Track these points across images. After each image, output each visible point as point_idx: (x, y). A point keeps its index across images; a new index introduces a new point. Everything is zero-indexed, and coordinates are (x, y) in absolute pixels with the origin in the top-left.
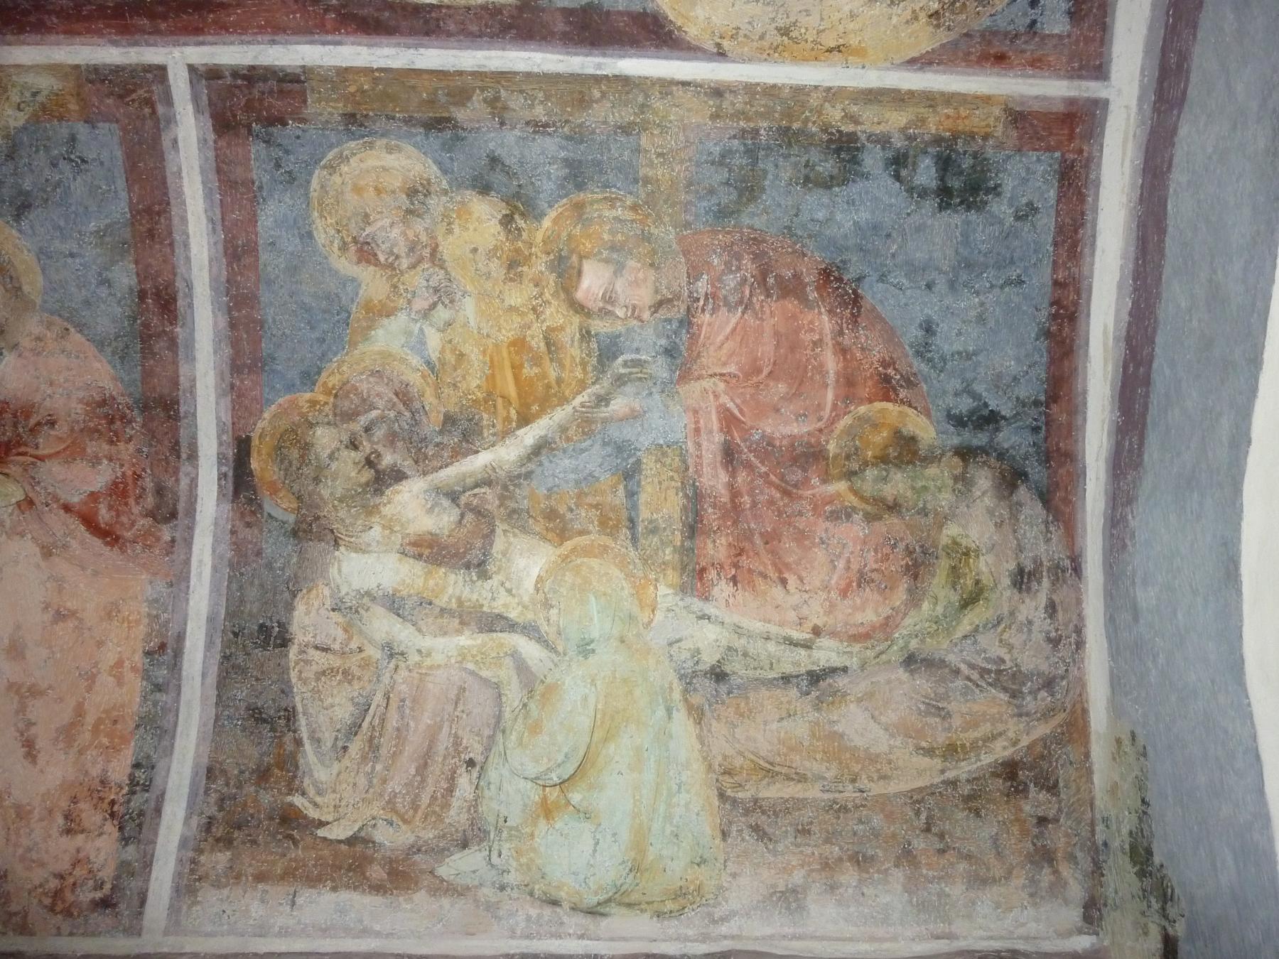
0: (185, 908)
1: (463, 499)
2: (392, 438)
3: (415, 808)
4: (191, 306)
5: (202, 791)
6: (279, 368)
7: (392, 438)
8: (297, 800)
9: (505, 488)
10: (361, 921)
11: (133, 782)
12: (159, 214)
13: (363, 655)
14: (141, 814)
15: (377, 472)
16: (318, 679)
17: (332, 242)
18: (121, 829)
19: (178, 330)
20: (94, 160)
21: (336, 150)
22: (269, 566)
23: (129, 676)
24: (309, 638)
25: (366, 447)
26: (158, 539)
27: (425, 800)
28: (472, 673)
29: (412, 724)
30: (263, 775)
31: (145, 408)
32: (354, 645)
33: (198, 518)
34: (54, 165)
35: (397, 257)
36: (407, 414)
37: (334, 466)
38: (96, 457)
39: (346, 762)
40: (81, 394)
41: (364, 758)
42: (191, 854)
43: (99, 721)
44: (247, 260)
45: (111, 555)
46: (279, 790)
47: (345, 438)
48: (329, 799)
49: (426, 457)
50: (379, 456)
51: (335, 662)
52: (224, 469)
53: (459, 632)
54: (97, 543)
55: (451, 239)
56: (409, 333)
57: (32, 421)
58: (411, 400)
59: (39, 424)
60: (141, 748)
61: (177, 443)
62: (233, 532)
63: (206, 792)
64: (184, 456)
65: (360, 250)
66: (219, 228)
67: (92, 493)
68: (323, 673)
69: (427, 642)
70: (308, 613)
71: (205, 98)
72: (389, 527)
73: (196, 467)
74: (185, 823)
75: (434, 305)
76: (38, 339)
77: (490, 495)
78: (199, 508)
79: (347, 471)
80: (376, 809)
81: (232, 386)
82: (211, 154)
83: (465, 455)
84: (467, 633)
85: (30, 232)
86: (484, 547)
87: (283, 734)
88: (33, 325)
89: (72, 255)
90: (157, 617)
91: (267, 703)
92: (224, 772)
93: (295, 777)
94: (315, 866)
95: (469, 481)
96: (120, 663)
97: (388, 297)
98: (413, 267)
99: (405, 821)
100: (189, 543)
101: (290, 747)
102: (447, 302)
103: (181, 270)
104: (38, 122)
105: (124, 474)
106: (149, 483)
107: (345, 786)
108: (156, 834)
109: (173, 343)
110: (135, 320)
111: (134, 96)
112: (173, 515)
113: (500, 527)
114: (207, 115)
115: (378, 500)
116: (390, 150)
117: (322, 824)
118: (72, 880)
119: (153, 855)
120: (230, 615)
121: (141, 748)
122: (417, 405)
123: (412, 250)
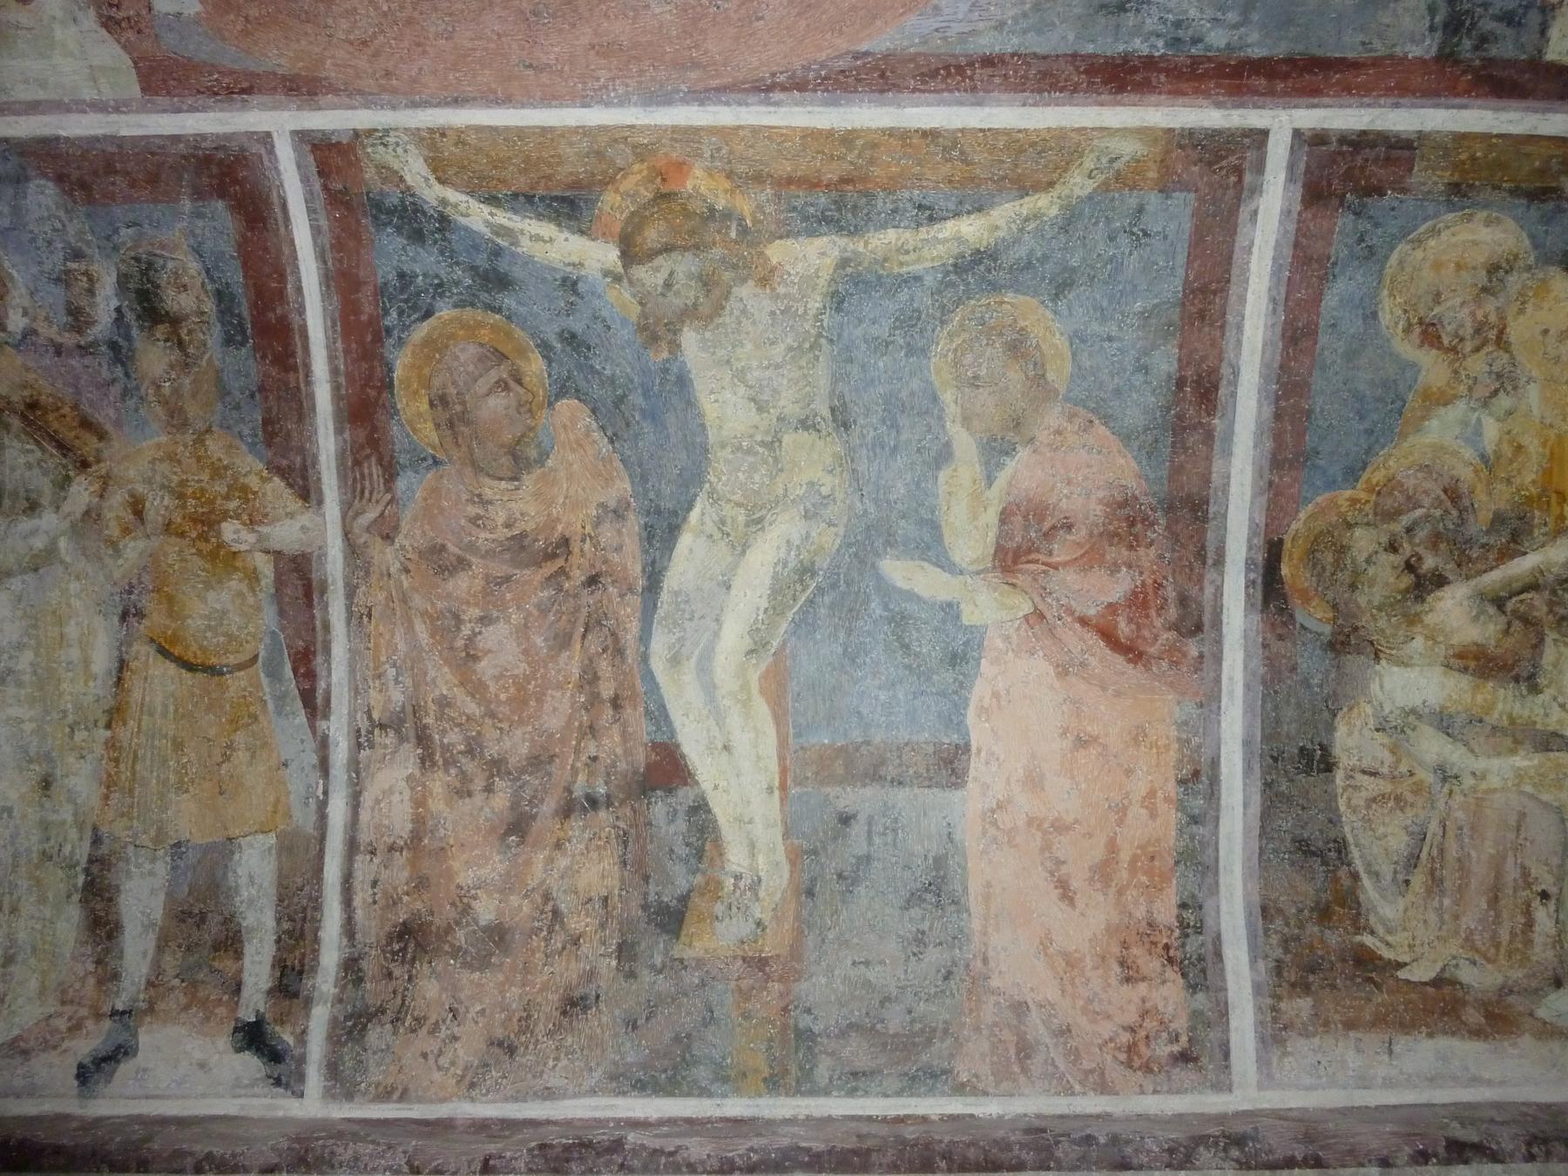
0: (1275, 1060)
1: (1510, 606)
2: (1436, 540)
3: (1497, 946)
4: (1234, 395)
5: (1261, 932)
6: (1322, 463)
7: (1436, 540)
8: (1368, 940)
9: (1554, 592)
10: (1467, 1069)
11: (1183, 925)
12: (1215, 293)
13: (1415, 779)
14: (1201, 959)
15: (1418, 576)
16: (1368, 807)
17: (1397, 324)
18: (1184, 975)
19: (1216, 421)
20: (1158, 233)
21: (1430, 223)
22: (1306, 683)
23: (1162, 807)
24: (1354, 761)
25: (1407, 549)
26: (1185, 655)
27: (1505, 936)
28: (1532, 797)
29: (1473, 854)
30: (1324, 914)
31: (1170, 509)
32: (1403, 768)
33: (1225, 630)
34: (1112, 239)
35: (1462, 340)
36: (1455, 513)
37: (1371, 571)
38: (1115, 564)
39: (1410, 897)
40: (1101, 494)
41: (1429, 891)
42: (1269, 1001)
43: (1134, 859)
44: (1304, 344)
45: (1134, 674)
46: (1345, 929)
47: (1384, 540)
48: (1398, 938)
49: (1470, 560)
50: (1420, 559)
51: (1386, 787)
52: (1252, 576)
53: (1513, 752)
54: (1119, 661)
55: (1522, 319)
56: (1465, 424)
57: (1047, 525)
58: (1459, 497)
59: (1054, 527)
60: (1184, 887)
61: (1203, 547)
62: (1265, 646)
63: (1266, 931)
64: (1210, 562)
65: (1424, 332)
66: (1281, 308)
67: (1110, 605)
68: (1374, 800)
69: (1481, 764)
70: (1350, 734)
71: (1302, 166)
72: (1431, 638)
73: (1222, 574)
74: (1251, 968)
75: (1496, 392)
76: (1058, 432)
77: (1538, 603)
78: (1225, 620)
79: (1385, 576)
80: (1454, 947)
81: (1271, 483)
82: (1292, 227)
83: (1512, 557)
84: (1522, 753)
85: (1066, 313)
86: (1533, 658)
87: (1337, 868)
88: (1054, 417)
89: (1110, 339)
90: (1188, 741)
91: (1312, 833)
92: (1280, 911)
93: (1359, 914)
94: (1406, 1010)
95: (1516, 586)
96: (1152, 794)
97: (1448, 384)
98: (1477, 350)
99: (1489, 960)
100: (1218, 659)
101: (1346, 882)
102: (1509, 388)
103: (1230, 355)
104: (1107, 190)
105: (1143, 584)
106: (1171, 593)
107: (1414, 923)
108: (1224, 980)
109: (1209, 436)
110: (1169, 409)
111: (1224, 163)
112: (1199, 628)
113: (1551, 636)
114: (1300, 184)
115: (1419, 608)
116: (1488, 223)
117: (1400, 965)
118: (1143, 1033)
119: (1226, 1003)
120: (1266, 738)
121: (1184, 887)
122: (1466, 502)
123: (1478, 331)
